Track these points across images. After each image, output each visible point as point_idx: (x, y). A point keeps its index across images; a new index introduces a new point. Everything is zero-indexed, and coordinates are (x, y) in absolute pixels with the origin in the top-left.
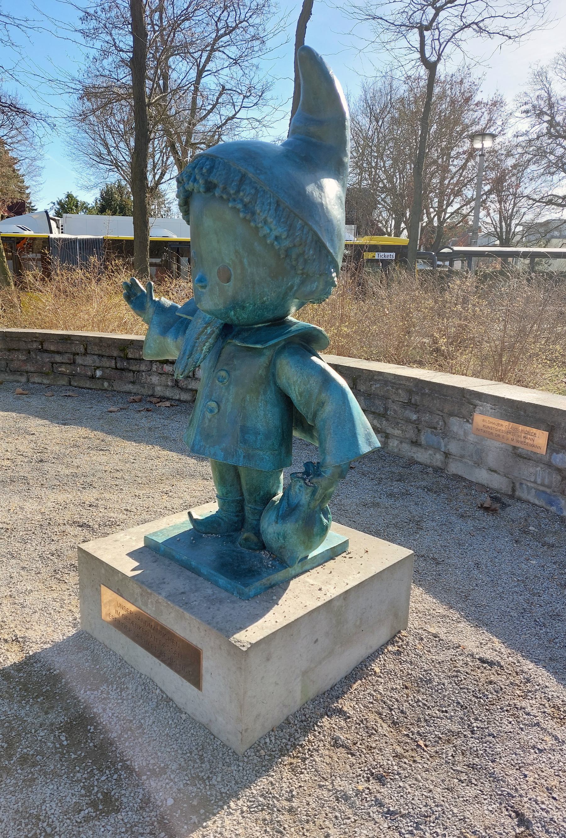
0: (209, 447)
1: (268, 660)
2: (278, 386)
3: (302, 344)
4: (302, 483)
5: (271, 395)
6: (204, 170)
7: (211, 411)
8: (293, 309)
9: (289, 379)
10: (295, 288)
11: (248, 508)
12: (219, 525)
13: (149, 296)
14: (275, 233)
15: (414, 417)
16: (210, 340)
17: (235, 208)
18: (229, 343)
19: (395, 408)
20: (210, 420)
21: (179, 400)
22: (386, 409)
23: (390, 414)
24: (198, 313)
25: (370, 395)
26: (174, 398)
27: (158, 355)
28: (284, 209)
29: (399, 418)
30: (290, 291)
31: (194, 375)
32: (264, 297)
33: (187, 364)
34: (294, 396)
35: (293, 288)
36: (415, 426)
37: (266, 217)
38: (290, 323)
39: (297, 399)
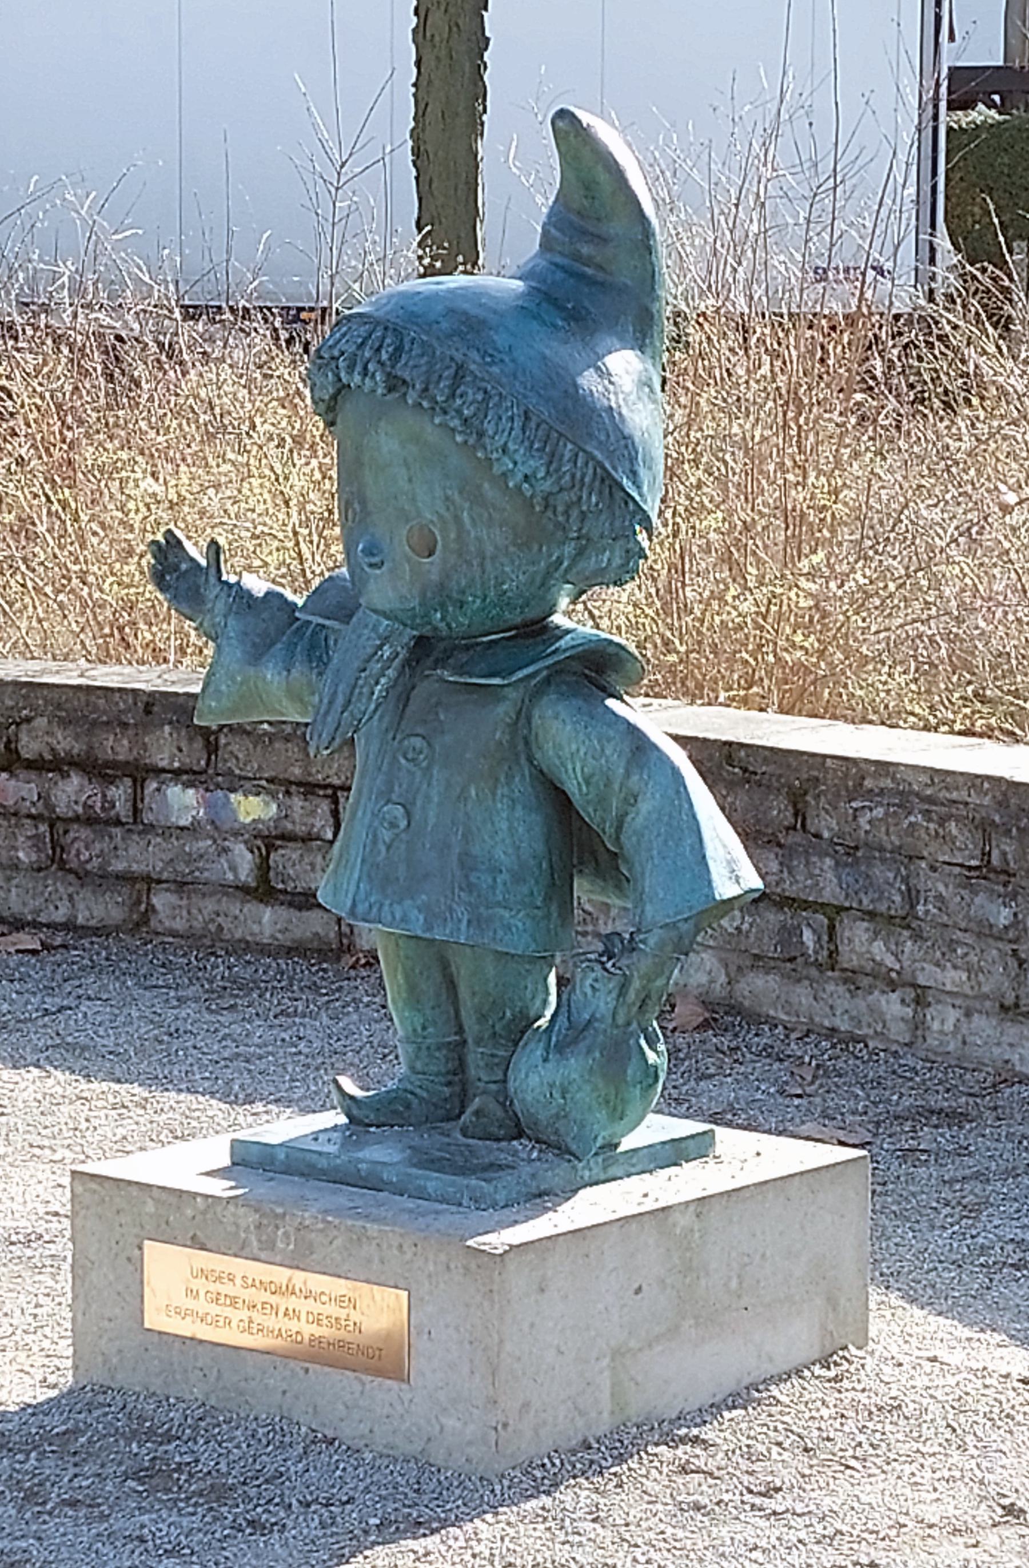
0: (391, 905)
1: (542, 1290)
2: (535, 767)
3: (586, 676)
4: (599, 972)
5: (522, 785)
6: (384, 356)
7: (393, 825)
8: (564, 603)
9: (561, 747)
10: (566, 564)
11: (475, 1057)
12: (408, 1106)
13: (213, 571)
14: (523, 470)
15: (1003, 916)
16: (390, 672)
17: (447, 426)
18: (427, 676)
19: (941, 888)
20: (389, 847)
21: (69, 926)
22: (911, 897)
23: (927, 912)
24: (359, 614)
25: (856, 848)
26: (43, 919)
27: (234, 711)
28: (538, 426)
29: (955, 926)
30: (556, 569)
31: (136, 811)
32: (503, 583)
33: (339, 724)
34: (572, 787)
35: (561, 564)
36: (1009, 948)
37: (506, 443)
38: (557, 632)
39: (580, 790)
